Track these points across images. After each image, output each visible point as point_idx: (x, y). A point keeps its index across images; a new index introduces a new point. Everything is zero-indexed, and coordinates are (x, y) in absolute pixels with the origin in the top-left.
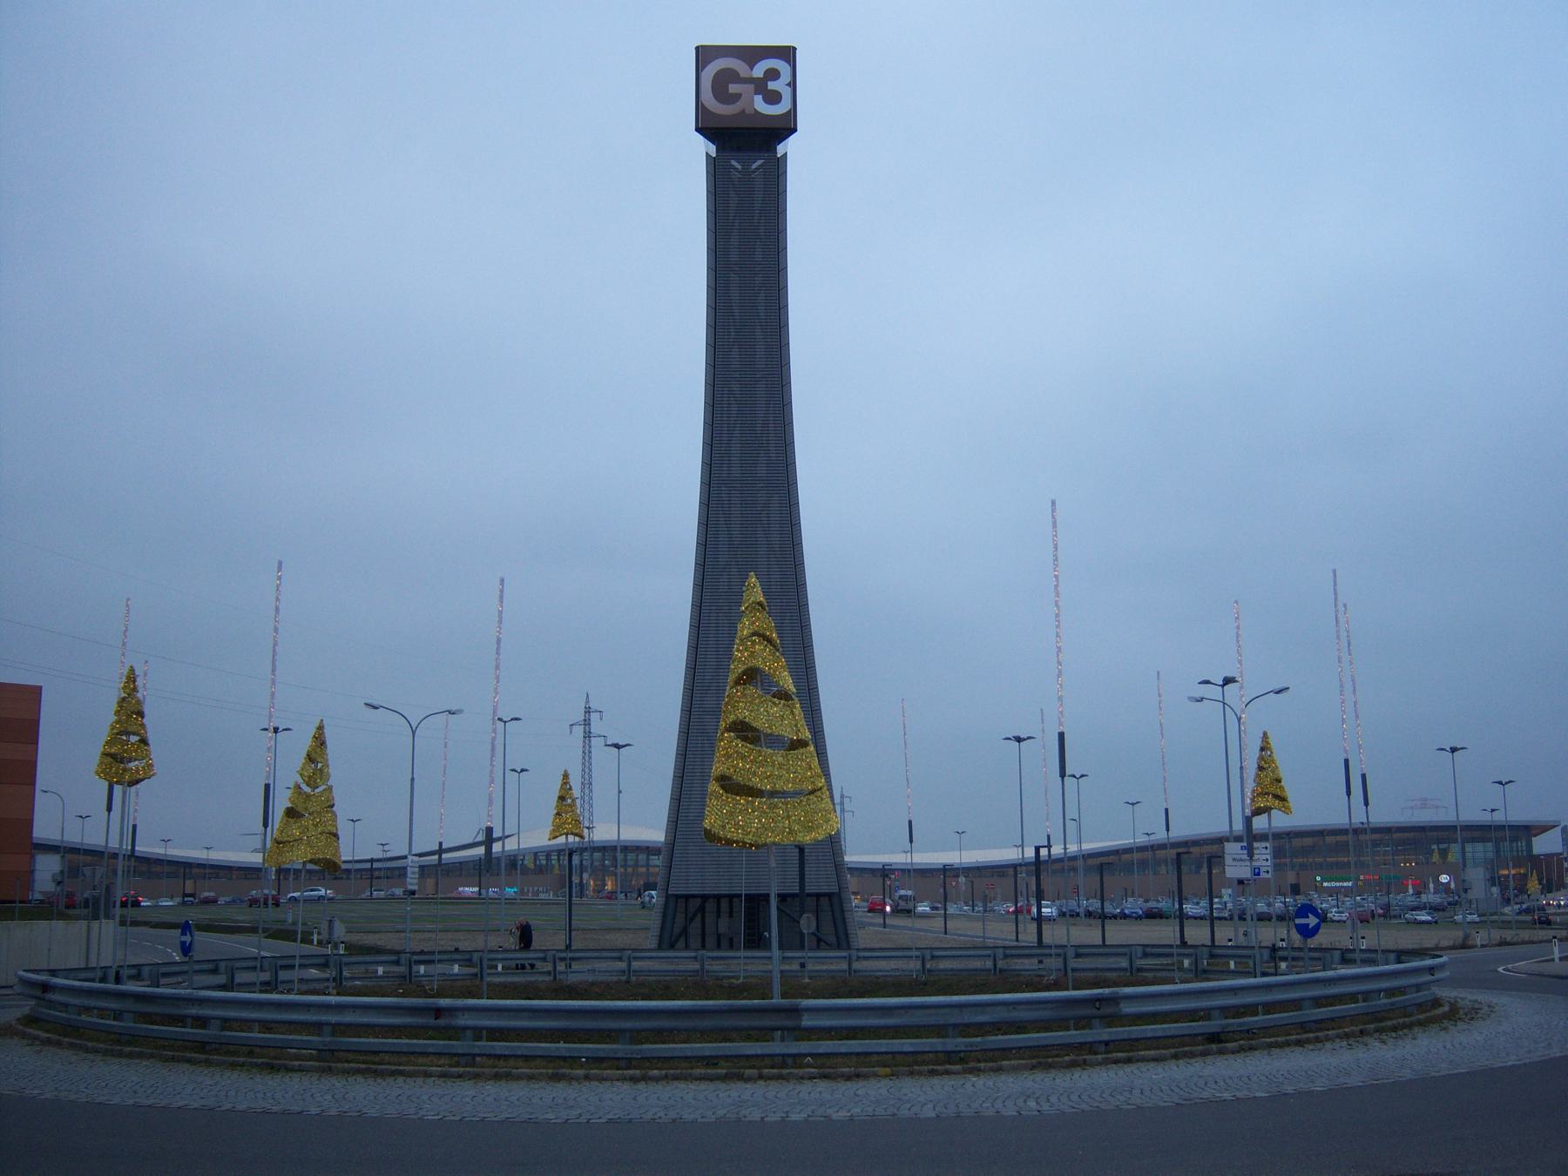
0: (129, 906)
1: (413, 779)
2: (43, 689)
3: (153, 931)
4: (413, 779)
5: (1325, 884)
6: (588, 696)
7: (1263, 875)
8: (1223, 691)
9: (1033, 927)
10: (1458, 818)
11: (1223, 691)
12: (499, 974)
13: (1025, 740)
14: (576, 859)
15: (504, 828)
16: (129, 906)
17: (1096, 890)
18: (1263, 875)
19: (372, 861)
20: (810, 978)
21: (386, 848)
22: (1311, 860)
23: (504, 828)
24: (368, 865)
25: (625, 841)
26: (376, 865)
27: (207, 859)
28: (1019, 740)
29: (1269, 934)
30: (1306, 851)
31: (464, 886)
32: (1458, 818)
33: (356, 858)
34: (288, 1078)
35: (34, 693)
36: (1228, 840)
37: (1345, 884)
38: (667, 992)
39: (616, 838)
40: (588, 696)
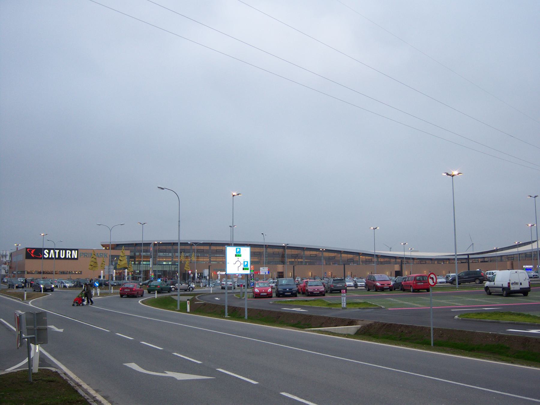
0: (43, 259)
1: (179, 221)
4: (179, 221)
7: (266, 274)
8: (452, 178)
11: (452, 178)
12: (344, 308)
14: (521, 255)
15: (532, 246)
16: (43, 259)
18: (266, 274)
19: (468, 255)
20: (507, 338)
22: (296, 260)
23: (532, 246)
24: (466, 257)
26: (470, 256)
30: (202, 252)
33: (457, 254)
36: (229, 245)
39: (177, 239)
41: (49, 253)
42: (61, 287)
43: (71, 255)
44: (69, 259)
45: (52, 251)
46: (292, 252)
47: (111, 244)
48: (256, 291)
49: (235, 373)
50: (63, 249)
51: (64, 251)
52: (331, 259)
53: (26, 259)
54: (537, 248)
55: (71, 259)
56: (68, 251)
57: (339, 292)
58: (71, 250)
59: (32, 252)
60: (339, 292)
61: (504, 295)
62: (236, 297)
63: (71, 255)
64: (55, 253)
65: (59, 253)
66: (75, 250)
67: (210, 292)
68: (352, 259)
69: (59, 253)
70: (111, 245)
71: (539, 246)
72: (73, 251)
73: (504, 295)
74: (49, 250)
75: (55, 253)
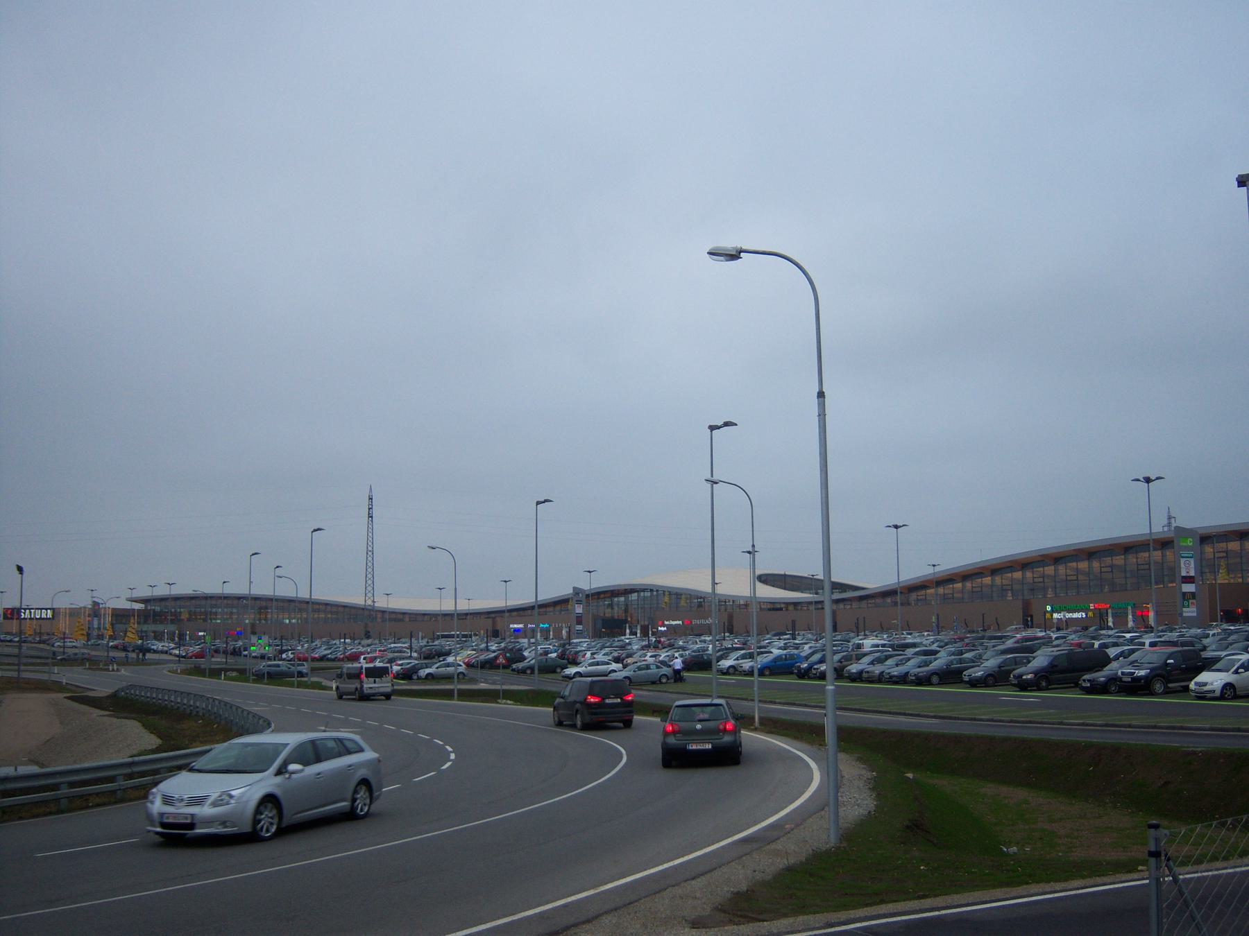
2: (1237, 185)
3: (881, 709)
5: (1055, 616)
6: (371, 489)
9: (413, 645)
10: (311, 596)
13: (901, 527)
17: (724, 623)
21: (95, 594)
25: (253, 595)
27: (170, 595)
28: (896, 527)
29: (158, 645)
31: (514, 624)
32: (311, 596)
34: (704, 933)
35: (1239, 187)
37: (1076, 615)
38: (1053, 724)
40: (371, 489)
41: (25, 613)
42: (834, 641)
43: (47, 615)
44: (44, 619)
45: (28, 611)
46: (1139, 560)
47: (1153, 537)
48: (854, 671)
49: (705, 855)
50: (38, 609)
51: (40, 611)
52: (1070, 581)
53: (1239, 187)
54: (1149, 532)
55: (47, 619)
56: (43, 611)
57: (1072, 685)
58: (46, 609)
59: (9, 612)
60: (1072, 685)
61: (579, 726)
62: (132, 675)
63: (47, 615)
64: (30, 612)
65: (35, 613)
66: (50, 609)
67: (60, 667)
68: (701, 598)
69: (35, 613)
70: (1154, 540)
71: (1152, 529)
72: (49, 611)
73: (579, 726)
74: (25, 609)
75: (30, 612)
